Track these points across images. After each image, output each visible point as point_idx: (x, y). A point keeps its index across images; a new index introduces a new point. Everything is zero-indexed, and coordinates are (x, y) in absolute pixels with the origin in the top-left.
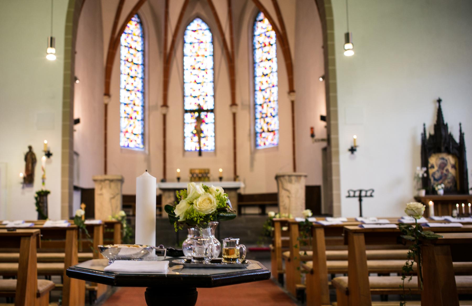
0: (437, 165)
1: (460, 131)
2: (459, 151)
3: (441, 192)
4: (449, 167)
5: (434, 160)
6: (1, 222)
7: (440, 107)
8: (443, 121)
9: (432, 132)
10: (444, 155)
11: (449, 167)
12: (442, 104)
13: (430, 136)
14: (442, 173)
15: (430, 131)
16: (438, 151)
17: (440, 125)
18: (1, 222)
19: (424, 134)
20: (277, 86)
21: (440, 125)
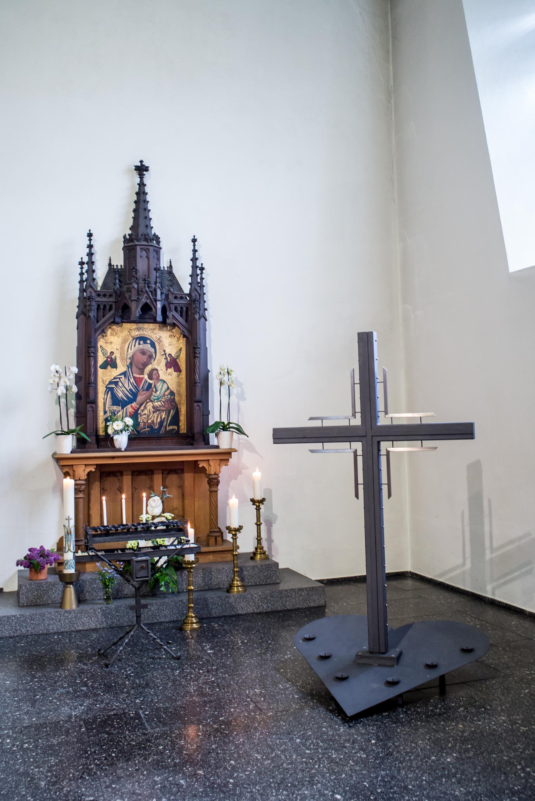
0: (122, 359)
1: (194, 259)
2: (187, 313)
3: (122, 441)
4: (159, 364)
5: (116, 342)
6: (2, 589)
7: (142, 185)
8: (148, 227)
9: (119, 261)
10: (150, 331)
11: (159, 364)
12: (149, 179)
13: (112, 270)
14: (138, 381)
15: (109, 254)
16: (122, 314)
17: (140, 239)
18: (2, 589)
19: (88, 264)
20: (87, 263)
21: (140, 239)
